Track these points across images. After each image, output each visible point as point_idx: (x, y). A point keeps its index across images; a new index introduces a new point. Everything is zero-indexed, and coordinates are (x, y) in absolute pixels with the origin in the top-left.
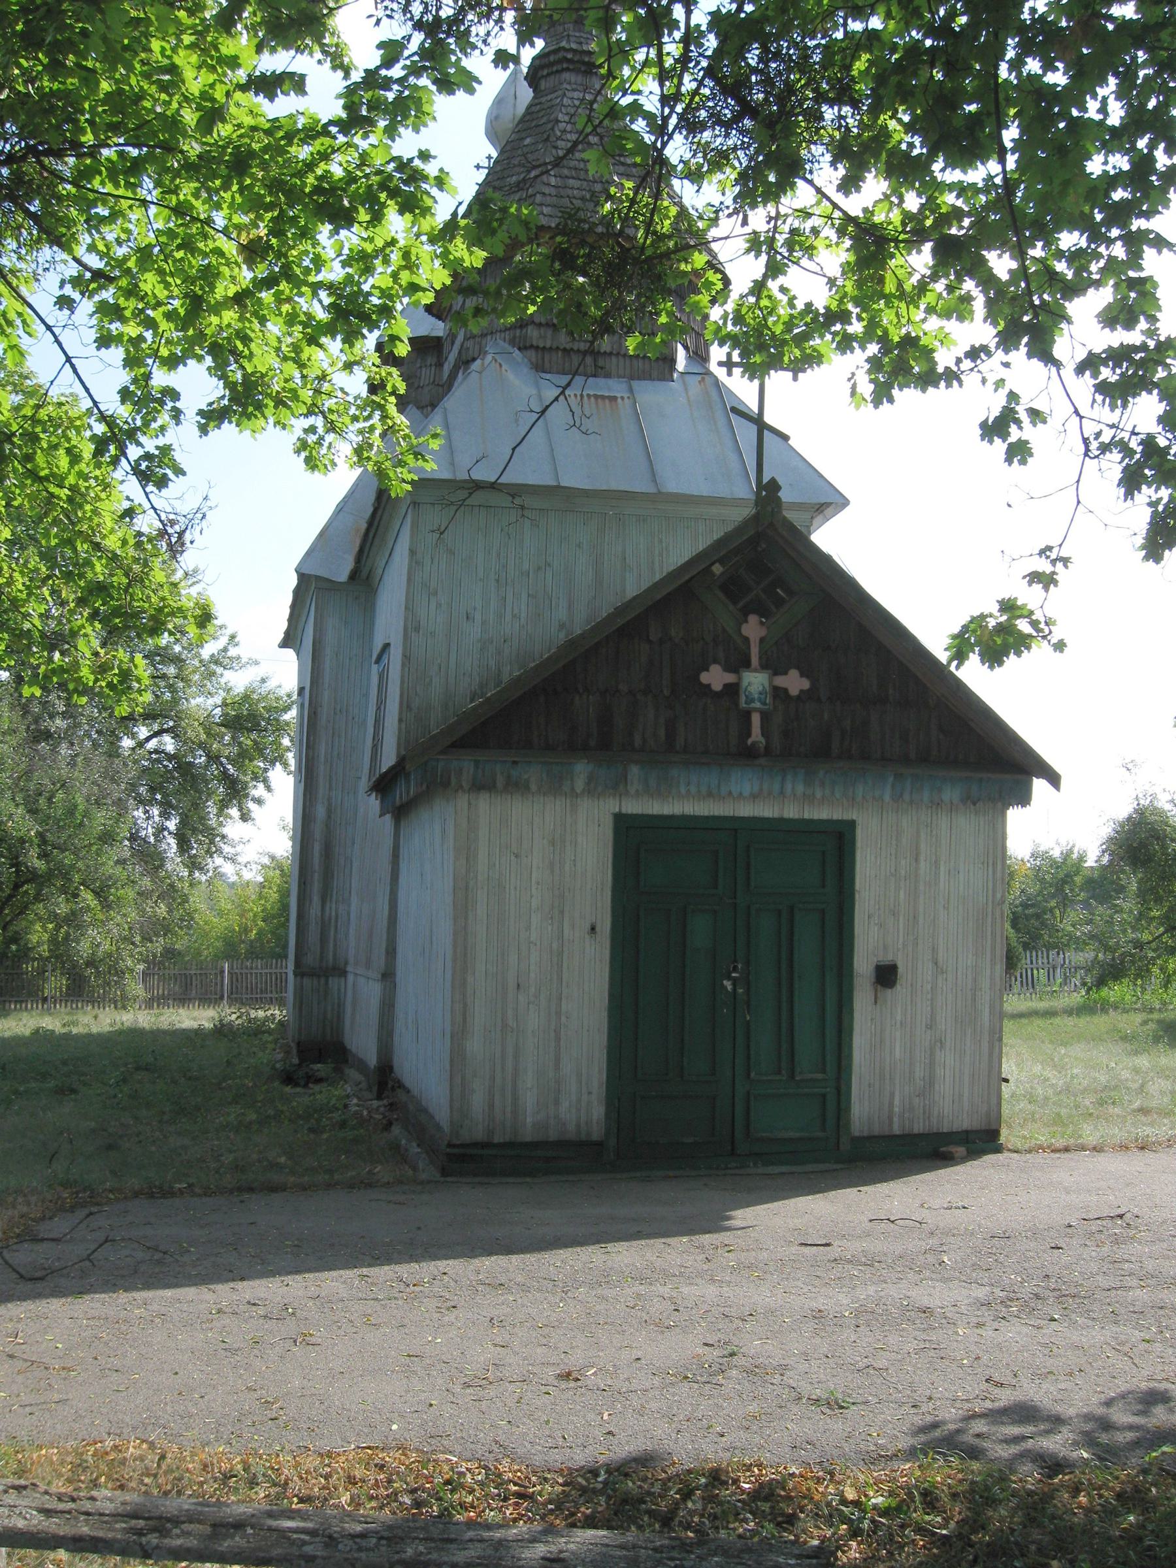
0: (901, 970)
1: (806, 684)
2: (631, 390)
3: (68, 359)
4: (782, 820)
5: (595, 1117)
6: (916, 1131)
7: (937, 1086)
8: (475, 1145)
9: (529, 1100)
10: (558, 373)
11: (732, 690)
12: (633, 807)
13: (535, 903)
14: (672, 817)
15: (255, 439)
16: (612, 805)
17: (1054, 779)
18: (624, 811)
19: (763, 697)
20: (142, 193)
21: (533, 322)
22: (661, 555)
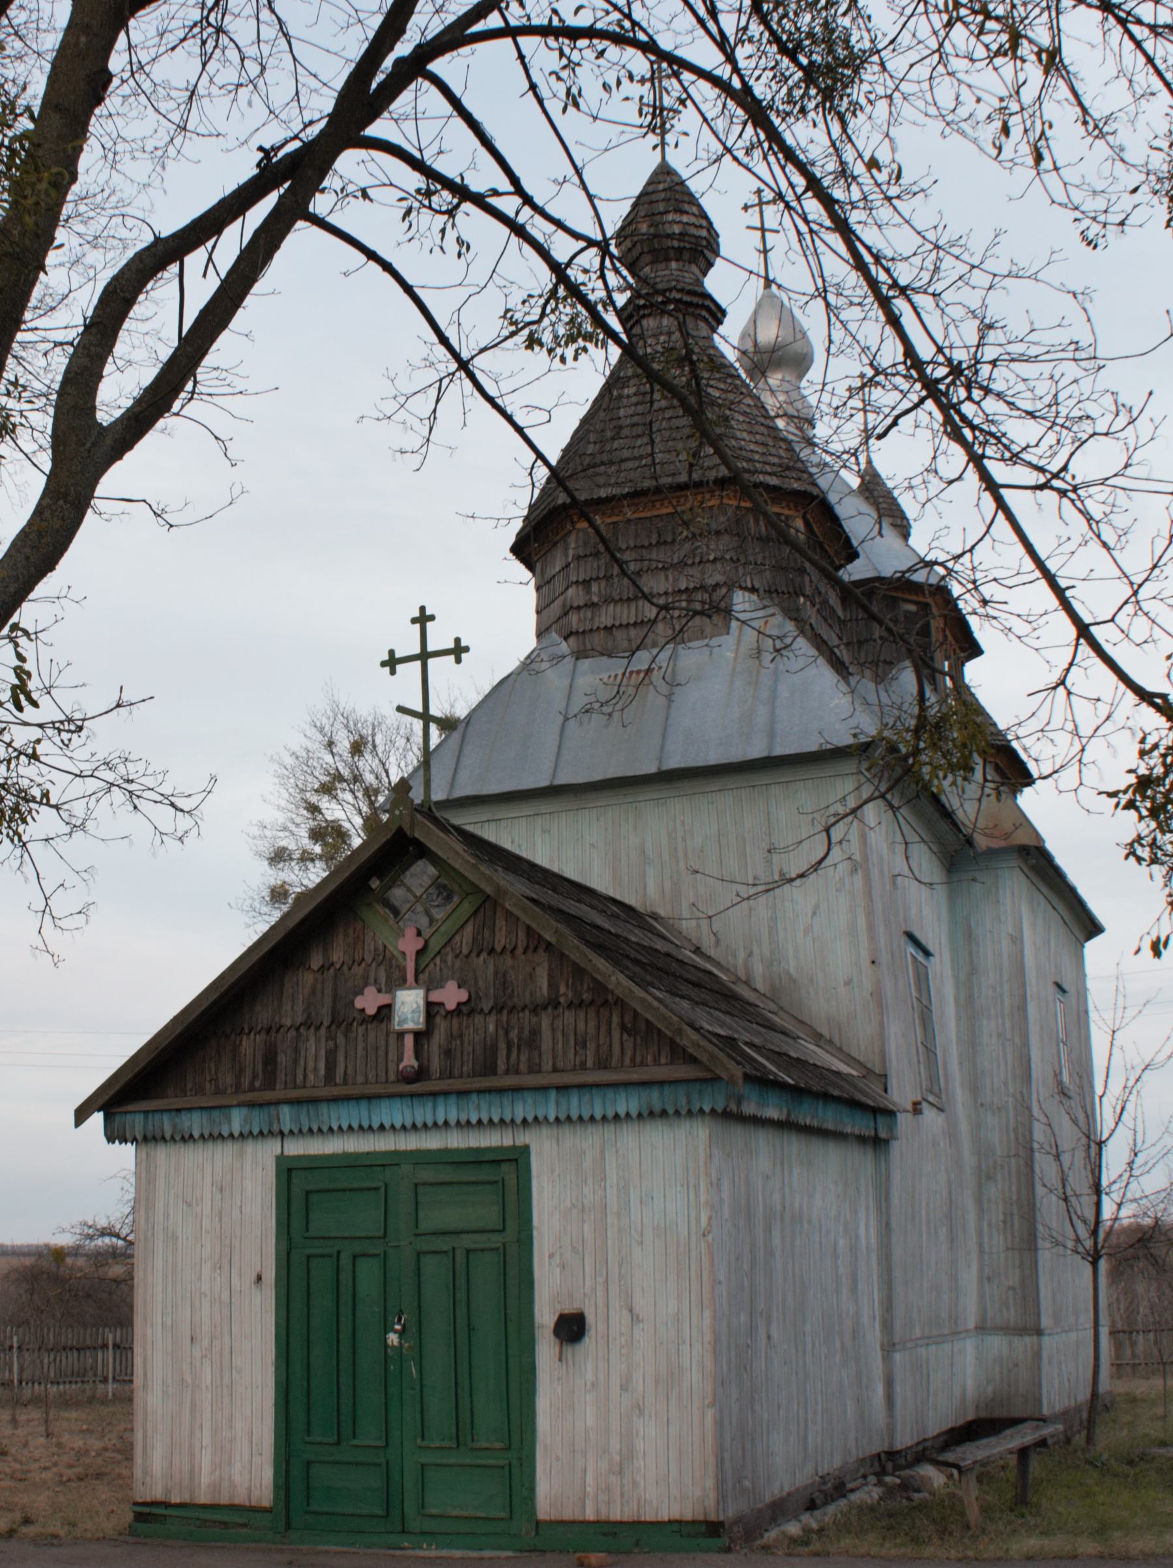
0: (590, 1318)
1: (463, 996)
3: (1083, 631)
6: (612, 1518)
9: (206, 1461)
11: (385, 1012)
12: (295, 1148)
15: (81, 1115)
18: (286, 1153)
19: (416, 1015)
21: (571, 607)
22: (684, 839)
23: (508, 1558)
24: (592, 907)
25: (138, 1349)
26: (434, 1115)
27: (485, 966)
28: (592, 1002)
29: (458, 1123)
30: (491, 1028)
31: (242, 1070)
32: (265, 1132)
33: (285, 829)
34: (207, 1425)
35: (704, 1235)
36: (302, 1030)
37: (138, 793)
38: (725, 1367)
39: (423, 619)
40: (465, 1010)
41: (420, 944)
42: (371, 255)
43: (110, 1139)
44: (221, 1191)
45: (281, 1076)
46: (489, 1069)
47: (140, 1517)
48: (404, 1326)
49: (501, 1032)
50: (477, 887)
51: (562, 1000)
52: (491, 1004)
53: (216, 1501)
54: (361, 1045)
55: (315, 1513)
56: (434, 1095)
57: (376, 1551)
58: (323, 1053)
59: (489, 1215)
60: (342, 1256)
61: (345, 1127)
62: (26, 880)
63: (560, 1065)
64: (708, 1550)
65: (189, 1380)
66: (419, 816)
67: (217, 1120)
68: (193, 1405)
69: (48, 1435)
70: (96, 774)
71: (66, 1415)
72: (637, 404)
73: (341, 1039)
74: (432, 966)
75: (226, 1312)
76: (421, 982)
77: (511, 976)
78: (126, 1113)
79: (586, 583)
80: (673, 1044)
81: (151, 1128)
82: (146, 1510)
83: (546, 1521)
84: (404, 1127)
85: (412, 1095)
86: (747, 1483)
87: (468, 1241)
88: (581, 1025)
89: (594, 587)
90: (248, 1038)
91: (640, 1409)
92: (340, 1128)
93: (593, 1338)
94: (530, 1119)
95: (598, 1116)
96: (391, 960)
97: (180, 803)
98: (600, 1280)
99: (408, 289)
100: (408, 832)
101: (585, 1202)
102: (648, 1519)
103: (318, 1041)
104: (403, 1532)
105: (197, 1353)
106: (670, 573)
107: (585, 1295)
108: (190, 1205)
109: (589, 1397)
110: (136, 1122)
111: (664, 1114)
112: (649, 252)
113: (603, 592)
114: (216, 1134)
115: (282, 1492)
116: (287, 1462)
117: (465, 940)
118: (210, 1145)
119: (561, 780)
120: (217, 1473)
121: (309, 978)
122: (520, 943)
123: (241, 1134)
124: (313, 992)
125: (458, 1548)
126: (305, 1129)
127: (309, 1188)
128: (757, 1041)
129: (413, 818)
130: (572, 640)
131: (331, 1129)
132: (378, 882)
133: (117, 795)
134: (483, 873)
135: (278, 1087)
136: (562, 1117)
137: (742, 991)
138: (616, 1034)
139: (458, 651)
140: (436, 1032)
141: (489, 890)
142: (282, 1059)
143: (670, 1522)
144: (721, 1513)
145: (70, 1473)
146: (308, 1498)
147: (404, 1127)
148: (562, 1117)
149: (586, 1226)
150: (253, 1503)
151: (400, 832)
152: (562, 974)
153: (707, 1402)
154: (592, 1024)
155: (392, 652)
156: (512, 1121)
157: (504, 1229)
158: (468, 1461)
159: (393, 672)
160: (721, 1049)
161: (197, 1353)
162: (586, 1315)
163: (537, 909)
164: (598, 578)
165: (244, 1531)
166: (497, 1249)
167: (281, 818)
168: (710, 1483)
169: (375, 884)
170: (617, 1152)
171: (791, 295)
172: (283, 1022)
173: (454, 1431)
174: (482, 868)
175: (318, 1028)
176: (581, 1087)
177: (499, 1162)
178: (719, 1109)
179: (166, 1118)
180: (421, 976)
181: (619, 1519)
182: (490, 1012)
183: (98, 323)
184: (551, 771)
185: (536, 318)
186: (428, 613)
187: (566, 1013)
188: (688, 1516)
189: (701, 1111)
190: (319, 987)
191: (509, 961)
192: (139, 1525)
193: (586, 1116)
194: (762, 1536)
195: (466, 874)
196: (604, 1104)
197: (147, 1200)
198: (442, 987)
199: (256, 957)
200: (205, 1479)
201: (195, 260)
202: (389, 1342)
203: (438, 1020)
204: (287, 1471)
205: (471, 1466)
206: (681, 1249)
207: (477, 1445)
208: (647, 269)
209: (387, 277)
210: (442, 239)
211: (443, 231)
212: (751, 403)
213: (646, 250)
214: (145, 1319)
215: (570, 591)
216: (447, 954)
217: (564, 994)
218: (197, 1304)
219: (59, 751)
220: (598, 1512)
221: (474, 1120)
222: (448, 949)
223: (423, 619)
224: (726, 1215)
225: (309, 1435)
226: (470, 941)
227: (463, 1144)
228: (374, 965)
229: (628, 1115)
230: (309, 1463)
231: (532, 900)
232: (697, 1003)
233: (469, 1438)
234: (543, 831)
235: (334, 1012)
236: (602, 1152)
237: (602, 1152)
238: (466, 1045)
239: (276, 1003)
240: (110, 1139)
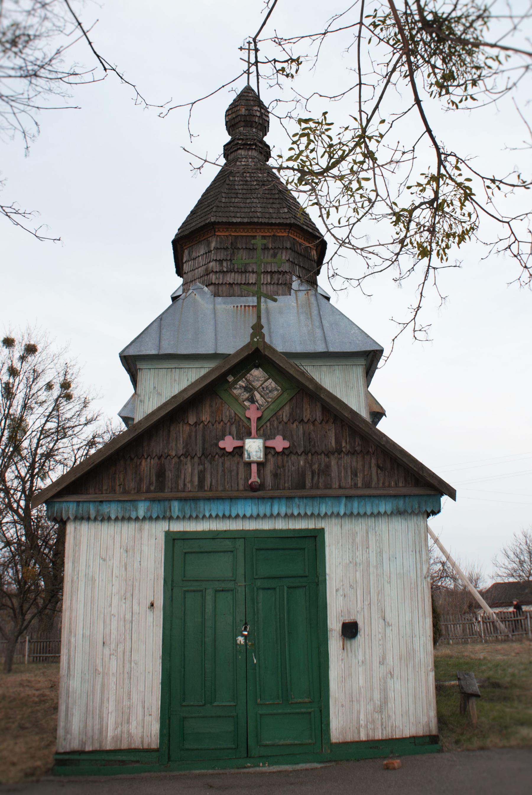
1: (287, 444)
4: (274, 530)
5: (153, 733)
7: (389, 705)
9: (111, 721)
10: (227, 296)
11: (240, 450)
12: (177, 527)
13: (115, 589)
16: (163, 527)
17: (452, 494)
18: (171, 530)
21: (212, 271)
26: (271, 510)
27: (299, 430)
30: (302, 463)
31: (141, 480)
34: (112, 698)
35: (425, 578)
36: (182, 458)
40: (287, 452)
44: (127, 551)
45: (169, 484)
46: (302, 486)
49: (307, 465)
51: (344, 450)
53: (118, 747)
58: (196, 472)
63: (343, 484)
65: (100, 669)
67: (128, 508)
68: (103, 686)
72: (243, 185)
74: (265, 427)
75: (128, 626)
77: (313, 435)
78: (63, 502)
79: (221, 261)
81: (80, 511)
88: (354, 464)
89: (225, 264)
90: (146, 461)
96: (239, 422)
98: (366, 603)
100: (262, 351)
102: (397, 737)
103: (193, 466)
107: (358, 612)
108: (104, 560)
109: (361, 669)
112: (244, 121)
113: (229, 267)
117: (285, 414)
118: (119, 524)
120: (119, 729)
124: (190, 436)
127: (185, 551)
132: (233, 378)
135: (166, 491)
142: (170, 475)
148: (348, 512)
149: (358, 573)
150: (146, 746)
152: (343, 436)
154: (360, 464)
158: (289, 711)
161: (107, 652)
162: (358, 623)
164: (226, 260)
168: (433, 713)
170: (376, 533)
172: (170, 453)
175: (192, 458)
181: (380, 738)
187: (346, 457)
188: (421, 733)
190: (193, 434)
191: (312, 427)
196: (372, 506)
197: (74, 556)
199: (163, 413)
205: (290, 714)
206: (413, 585)
213: (242, 120)
214: (71, 632)
215: (211, 264)
216: (274, 421)
220: (368, 735)
221: (296, 513)
222: (274, 418)
226: (288, 415)
227: (285, 527)
230: (184, 718)
235: (204, 449)
236: (367, 533)
237: (367, 533)
238: (287, 471)
239: (165, 442)
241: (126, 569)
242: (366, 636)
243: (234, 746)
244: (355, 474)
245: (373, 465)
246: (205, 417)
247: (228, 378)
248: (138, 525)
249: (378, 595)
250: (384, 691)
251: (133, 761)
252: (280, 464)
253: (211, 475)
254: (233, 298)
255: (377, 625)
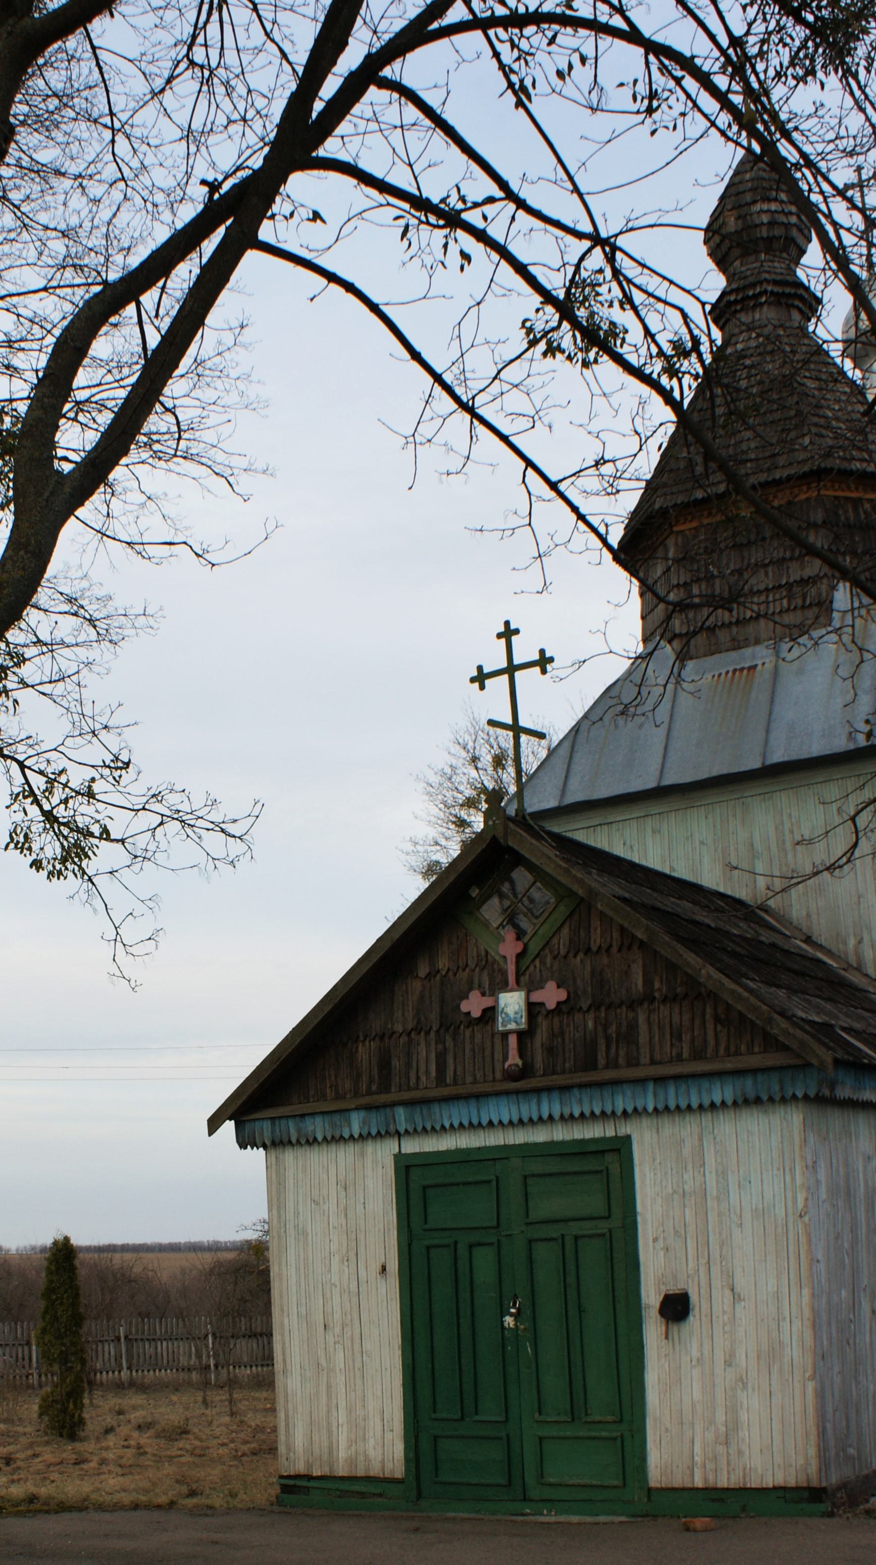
0: (694, 1298)
1: (562, 995)
2: (629, 658)
6: (719, 1485)
8: (298, 1477)
10: (705, 656)
11: (490, 1014)
12: (411, 1146)
13: (334, 1247)
14: (447, 1152)
15: (214, 1124)
18: (403, 1151)
20: (97, 825)
23: (621, 1523)
24: (694, 902)
25: (276, 1338)
26: (539, 1110)
28: (686, 995)
29: (562, 1117)
30: (590, 1025)
32: (383, 1133)
33: (437, 843)
34: (342, 1405)
35: (801, 1216)
37: (192, 822)
38: (825, 1342)
39: (508, 633)
40: (564, 1008)
41: (519, 947)
42: (332, 277)
43: (243, 1145)
47: (286, 1489)
48: (519, 1310)
49: (600, 1028)
50: (571, 891)
51: (657, 995)
52: (589, 1002)
53: (353, 1474)
54: (468, 1047)
55: (441, 1483)
56: (538, 1091)
57: (499, 1517)
58: (433, 1056)
59: (593, 1203)
60: (459, 1246)
61: (456, 1124)
62: (95, 910)
63: (657, 1057)
64: (811, 1515)
65: (323, 1363)
66: (511, 825)
68: (329, 1386)
69: (232, 1414)
70: (147, 807)
71: (257, 1395)
73: (449, 1042)
74: (532, 968)
75: (355, 1300)
76: (522, 984)
78: (255, 1120)
80: (766, 1035)
82: (291, 1482)
83: (657, 1489)
84: (511, 1123)
85: (517, 1092)
86: (851, 1451)
87: (575, 1228)
88: (676, 1019)
90: (364, 1045)
91: (743, 1382)
92: (452, 1125)
93: (698, 1316)
94: (630, 1110)
95: (695, 1105)
96: (493, 964)
97: (230, 828)
98: (703, 1261)
99: (374, 308)
100: (502, 841)
101: (686, 1187)
102: (753, 1486)
103: (428, 1045)
104: (525, 1500)
105: (331, 1339)
106: (770, 569)
110: (265, 1129)
111: (758, 1101)
114: (337, 1136)
115: (413, 1465)
116: (417, 1437)
117: (562, 942)
118: (333, 1147)
119: (668, 781)
120: (353, 1448)
121: (417, 985)
122: (614, 943)
123: (361, 1135)
124: (422, 997)
125: (574, 1514)
126: (419, 1129)
128: (857, 1026)
129: (506, 827)
130: (676, 643)
131: (443, 1127)
133: (173, 827)
134: (575, 876)
136: (660, 1107)
137: (854, 978)
138: (710, 1026)
139: (543, 662)
140: (539, 1031)
141: (581, 892)
142: (396, 1063)
143: (775, 1488)
144: (823, 1479)
145: (245, 1448)
146: (437, 1469)
147: (511, 1123)
148: (660, 1107)
151: (494, 839)
153: (807, 1375)
154: (686, 1017)
155: (480, 668)
156: (613, 1113)
157: (609, 1217)
159: (482, 687)
160: (813, 1036)
161: (331, 1339)
162: (690, 1295)
163: (628, 909)
165: (380, 1500)
166: (603, 1235)
167: (432, 833)
168: (812, 1452)
169: (475, 892)
170: (715, 1139)
171: (809, 271)
172: (395, 1028)
173: (568, 1406)
174: (574, 872)
175: (428, 1033)
176: (677, 1078)
177: (603, 1152)
178: (812, 1094)
179: (291, 1124)
180: (522, 979)
182: (589, 1010)
183: (51, 374)
184: (658, 773)
185: (555, 324)
186: (513, 627)
187: (662, 1007)
188: (792, 1483)
189: (794, 1097)
190: (427, 994)
191: (605, 960)
192: (285, 1496)
193: (683, 1105)
194: (867, 1501)
195: (559, 878)
198: (542, 988)
200: (342, 1454)
201: (149, 299)
202: (506, 1325)
203: (540, 1019)
204: (416, 1446)
206: (779, 1230)
207: (589, 1419)
208: (737, 263)
209: (351, 297)
210: (445, 253)
211: (445, 246)
212: (848, 390)
214: (282, 1310)
217: (659, 990)
218: (328, 1295)
219: (112, 788)
220: (706, 1479)
221: (577, 1114)
222: (547, 951)
223: (508, 633)
224: (823, 1195)
225: (435, 1412)
226: (567, 943)
227: (568, 1137)
228: (477, 970)
229: (723, 1103)
231: (624, 900)
232: (795, 992)
233: (583, 1415)
234: (653, 832)
236: (701, 1139)
237: (701, 1139)
238: (567, 1041)
240: (243, 1145)
241: (346, 1215)
242: (703, 1318)
243: (504, 1482)
244: (677, 1036)
245: (708, 1017)
246: (443, 963)
247: (470, 892)
248: (358, 1147)
249: (721, 1248)
250: (733, 1409)
251: (375, 1495)
252: (556, 1030)
253: (455, 1059)
254: (717, 656)
255: (721, 1299)
